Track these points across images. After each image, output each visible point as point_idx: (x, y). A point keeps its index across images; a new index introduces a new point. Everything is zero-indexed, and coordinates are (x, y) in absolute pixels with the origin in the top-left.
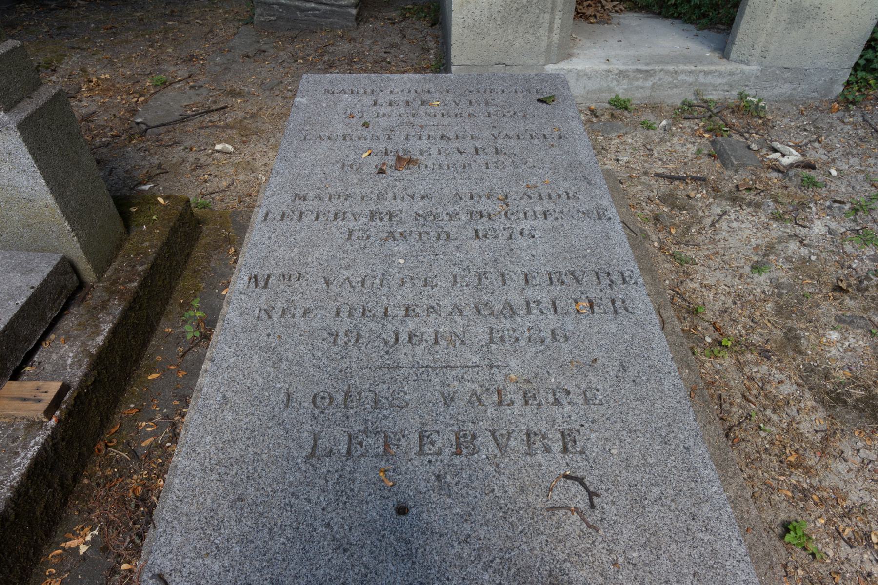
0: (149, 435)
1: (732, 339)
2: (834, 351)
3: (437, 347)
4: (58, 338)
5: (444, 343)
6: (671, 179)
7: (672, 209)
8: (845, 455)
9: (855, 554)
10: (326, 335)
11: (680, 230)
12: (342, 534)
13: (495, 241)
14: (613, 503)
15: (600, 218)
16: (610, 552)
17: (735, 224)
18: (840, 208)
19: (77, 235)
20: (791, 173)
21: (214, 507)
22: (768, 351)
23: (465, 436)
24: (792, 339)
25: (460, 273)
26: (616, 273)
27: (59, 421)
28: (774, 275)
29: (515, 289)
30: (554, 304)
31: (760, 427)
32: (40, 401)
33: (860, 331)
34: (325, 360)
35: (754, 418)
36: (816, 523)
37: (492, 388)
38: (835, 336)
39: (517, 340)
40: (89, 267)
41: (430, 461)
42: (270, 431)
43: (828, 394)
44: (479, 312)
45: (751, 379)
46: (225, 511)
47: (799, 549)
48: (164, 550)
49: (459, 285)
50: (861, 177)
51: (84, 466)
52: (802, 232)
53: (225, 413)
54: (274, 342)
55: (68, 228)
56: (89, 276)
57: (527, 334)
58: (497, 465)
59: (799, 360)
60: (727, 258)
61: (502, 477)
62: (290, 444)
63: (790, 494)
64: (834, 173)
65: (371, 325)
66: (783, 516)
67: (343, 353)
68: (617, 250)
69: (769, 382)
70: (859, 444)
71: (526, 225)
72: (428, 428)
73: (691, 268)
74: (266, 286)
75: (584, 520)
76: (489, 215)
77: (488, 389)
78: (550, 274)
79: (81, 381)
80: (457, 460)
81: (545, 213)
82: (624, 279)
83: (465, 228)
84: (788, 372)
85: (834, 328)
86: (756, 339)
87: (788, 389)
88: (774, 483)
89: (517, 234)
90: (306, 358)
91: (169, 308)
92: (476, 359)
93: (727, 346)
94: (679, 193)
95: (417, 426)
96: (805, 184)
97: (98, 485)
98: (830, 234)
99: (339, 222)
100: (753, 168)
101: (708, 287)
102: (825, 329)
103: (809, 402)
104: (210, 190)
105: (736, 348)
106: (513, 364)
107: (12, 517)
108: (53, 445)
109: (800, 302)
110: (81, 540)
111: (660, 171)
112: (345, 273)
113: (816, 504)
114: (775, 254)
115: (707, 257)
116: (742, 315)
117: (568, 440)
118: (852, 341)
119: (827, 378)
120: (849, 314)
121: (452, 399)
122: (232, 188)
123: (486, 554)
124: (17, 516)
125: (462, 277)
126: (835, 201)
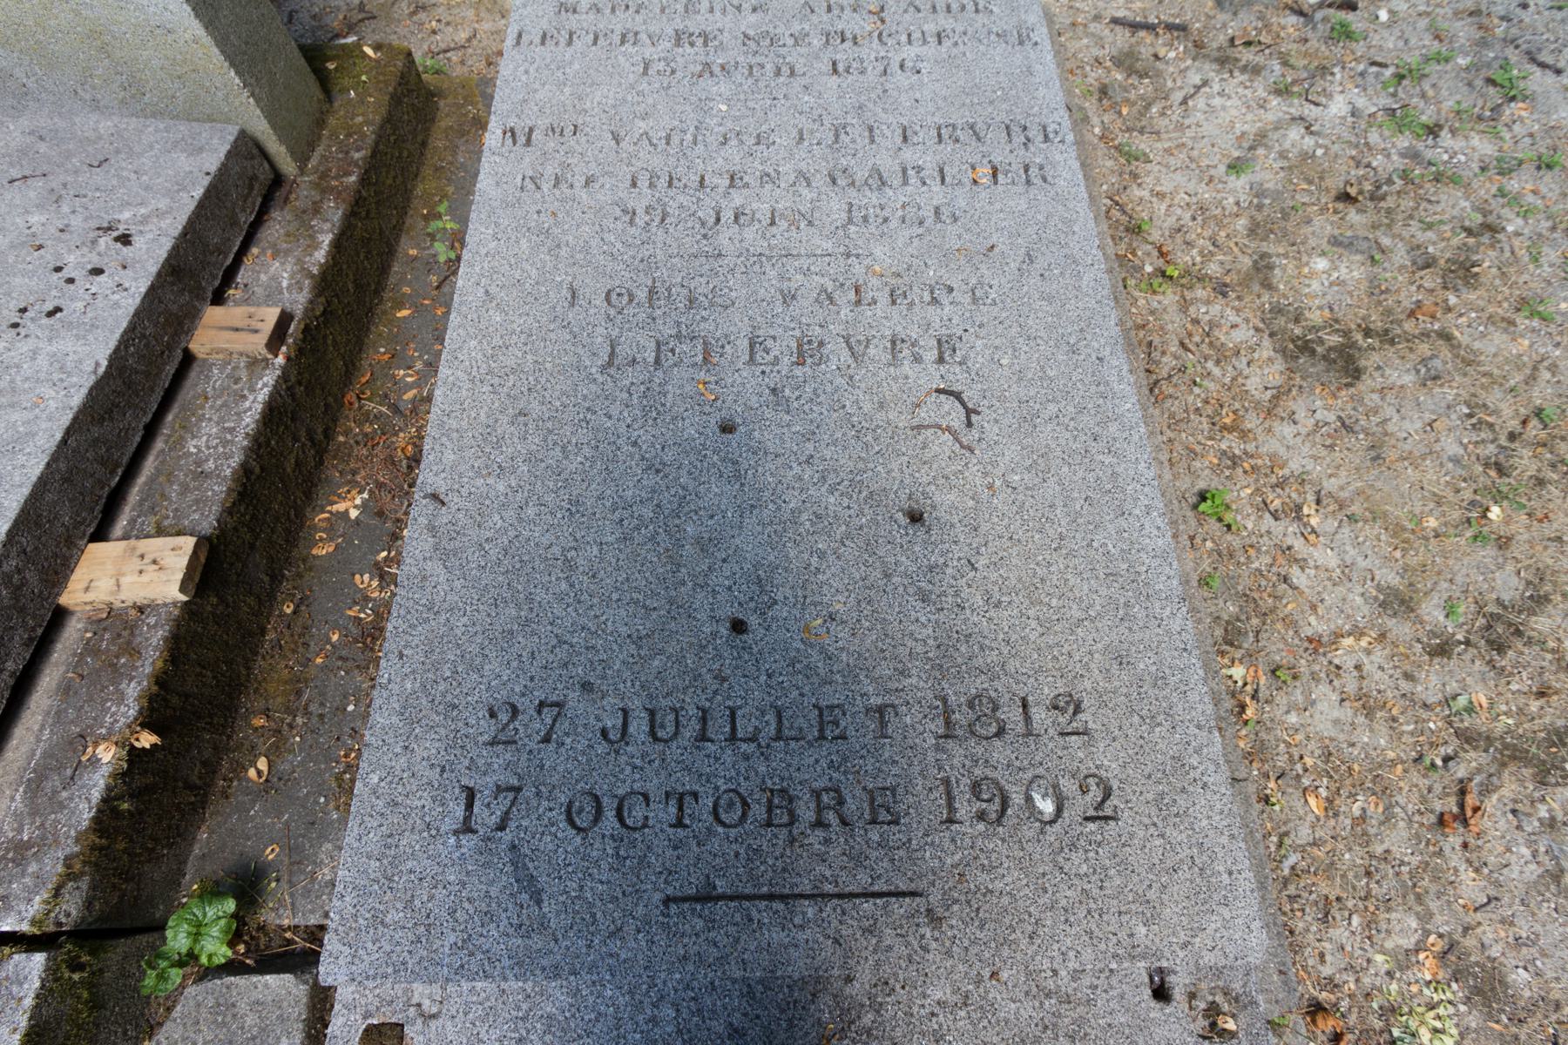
0: (410, 386)
1: (1181, 266)
2: (1315, 285)
3: (774, 230)
4: (263, 251)
5: (783, 224)
6: (1134, 27)
7: (1129, 76)
8: (1296, 417)
9: (1278, 528)
10: (618, 212)
11: (1135, 109)
12: (653, 453)
13: (861, 78)
14: (996, 421)
15: (1021, 43)
16: (986, 474)
17: (1217, 101)
18: (1377, 75)
19: (253, 95)
20: (1319, 15)
21: (491, 422)
22: (1226, 285)
23: (810, 342)
24: (1262, 269)
25: (807, 125)
26: (1036, 127)
27: (288, 359)
28: (1257, 178)
29: (888, 149)
30: (941, 171)
31: (1195, 383)
32: (256, 331)
33: (1358, 257)
34: (619, 245)
35: (1190, 371)
36: (1241, 492)
37: (848, 283)
38: (1321, 264)
39: (886, 220)
40: (283, 149)
41: (763, 372)
42: (553, 336)
43: (1293, 341)
44: (834, 182)
45: (1196, 322)
46: (504, 427)
47: (1213, 520)
48: (435, 468)
49: (806, 143)
50: (1423, 23)
51: (335, 421)
52: (1310, 111)
53: (491, 312)
54: (547, 221)
55: (237, 81)
56: (288, 166)
57: (900, 213)
58: (851, 378)
59: (1265, 298)
60: (1195, 153)
61: (857, 391)
62: (580, 351)
63: (1216, 461)
64: (1384, 15)
65: (681, 198)
66: (1201, 485)
67: (644, 236)
68: (1042, 91)
69: (1219, 326)
70: (1318, 403)
71: (909, 53)
72: (761, 333)
73: (1141, 168)
74: (528, 142)
75: (957, 439)
76: (855, 38)
77: (842, 285)
78: (939, 128)
79: (306, 309)
80: (798, 371)
81: (939, 35)
82: (1046, 136)
83: (817, 57)
84: (1248, 313)
85: (1323, 254)
86: (1213, 269)
87: (1243, 335)
88: (1198, 448)
89: (895, 67)
90: (594, 243)
91: (409, 221)
92: (828, 245)
93: (1171, 278)
94: (1143, 50)
95: (746, 330)
96: (1335, 34)
97: (357, 443)
98: (1353, 115)
99: (628, 47)
100: (1261, 8)
101: (1161, 196)
102: (1310, 256)
103: (1266, 350)
104: (443, 46)
105: (1184, 281)
106: (878, 252)
107: (257, 470)
108: (288, 389)
109: (1285, 217)
110: (349, 503)
111: (1120, 14)
112: (642, 124)
113: (1245, 472)
114: (1266, 146)
115: (1168, 151)
116: (1199, 235)
117: (945, 349)
118: (1344, 270)
119: (1297, 321)
120: (1349, 233)
121: (794, 297)
122: (475, 42)
123: (832, 475)
124: (262, 469)
125: (812, 132)
126: (1374, 64)
